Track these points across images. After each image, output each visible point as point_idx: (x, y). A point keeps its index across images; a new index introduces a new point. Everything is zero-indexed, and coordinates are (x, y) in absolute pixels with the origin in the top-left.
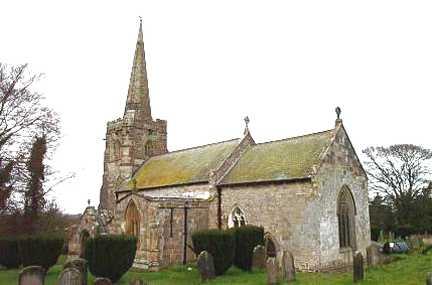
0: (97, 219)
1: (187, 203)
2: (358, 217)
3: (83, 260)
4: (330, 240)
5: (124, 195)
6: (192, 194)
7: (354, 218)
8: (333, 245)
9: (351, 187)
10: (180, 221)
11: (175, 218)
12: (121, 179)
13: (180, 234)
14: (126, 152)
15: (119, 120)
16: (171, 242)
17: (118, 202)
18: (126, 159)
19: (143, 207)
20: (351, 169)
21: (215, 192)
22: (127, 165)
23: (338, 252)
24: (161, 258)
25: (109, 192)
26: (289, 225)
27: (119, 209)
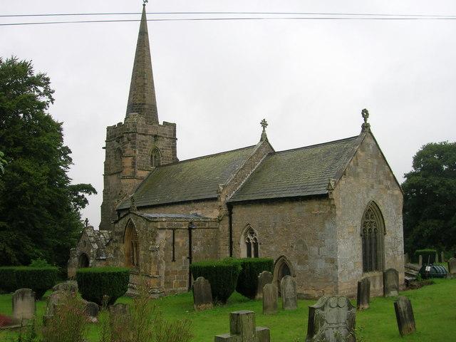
4: (351, 264)
7: (383, 239)
11: (177, 240)
13: (184, 258)
20: (380, 182)
24: (162, 284)
26: (305, 248)
27: (116, 230)
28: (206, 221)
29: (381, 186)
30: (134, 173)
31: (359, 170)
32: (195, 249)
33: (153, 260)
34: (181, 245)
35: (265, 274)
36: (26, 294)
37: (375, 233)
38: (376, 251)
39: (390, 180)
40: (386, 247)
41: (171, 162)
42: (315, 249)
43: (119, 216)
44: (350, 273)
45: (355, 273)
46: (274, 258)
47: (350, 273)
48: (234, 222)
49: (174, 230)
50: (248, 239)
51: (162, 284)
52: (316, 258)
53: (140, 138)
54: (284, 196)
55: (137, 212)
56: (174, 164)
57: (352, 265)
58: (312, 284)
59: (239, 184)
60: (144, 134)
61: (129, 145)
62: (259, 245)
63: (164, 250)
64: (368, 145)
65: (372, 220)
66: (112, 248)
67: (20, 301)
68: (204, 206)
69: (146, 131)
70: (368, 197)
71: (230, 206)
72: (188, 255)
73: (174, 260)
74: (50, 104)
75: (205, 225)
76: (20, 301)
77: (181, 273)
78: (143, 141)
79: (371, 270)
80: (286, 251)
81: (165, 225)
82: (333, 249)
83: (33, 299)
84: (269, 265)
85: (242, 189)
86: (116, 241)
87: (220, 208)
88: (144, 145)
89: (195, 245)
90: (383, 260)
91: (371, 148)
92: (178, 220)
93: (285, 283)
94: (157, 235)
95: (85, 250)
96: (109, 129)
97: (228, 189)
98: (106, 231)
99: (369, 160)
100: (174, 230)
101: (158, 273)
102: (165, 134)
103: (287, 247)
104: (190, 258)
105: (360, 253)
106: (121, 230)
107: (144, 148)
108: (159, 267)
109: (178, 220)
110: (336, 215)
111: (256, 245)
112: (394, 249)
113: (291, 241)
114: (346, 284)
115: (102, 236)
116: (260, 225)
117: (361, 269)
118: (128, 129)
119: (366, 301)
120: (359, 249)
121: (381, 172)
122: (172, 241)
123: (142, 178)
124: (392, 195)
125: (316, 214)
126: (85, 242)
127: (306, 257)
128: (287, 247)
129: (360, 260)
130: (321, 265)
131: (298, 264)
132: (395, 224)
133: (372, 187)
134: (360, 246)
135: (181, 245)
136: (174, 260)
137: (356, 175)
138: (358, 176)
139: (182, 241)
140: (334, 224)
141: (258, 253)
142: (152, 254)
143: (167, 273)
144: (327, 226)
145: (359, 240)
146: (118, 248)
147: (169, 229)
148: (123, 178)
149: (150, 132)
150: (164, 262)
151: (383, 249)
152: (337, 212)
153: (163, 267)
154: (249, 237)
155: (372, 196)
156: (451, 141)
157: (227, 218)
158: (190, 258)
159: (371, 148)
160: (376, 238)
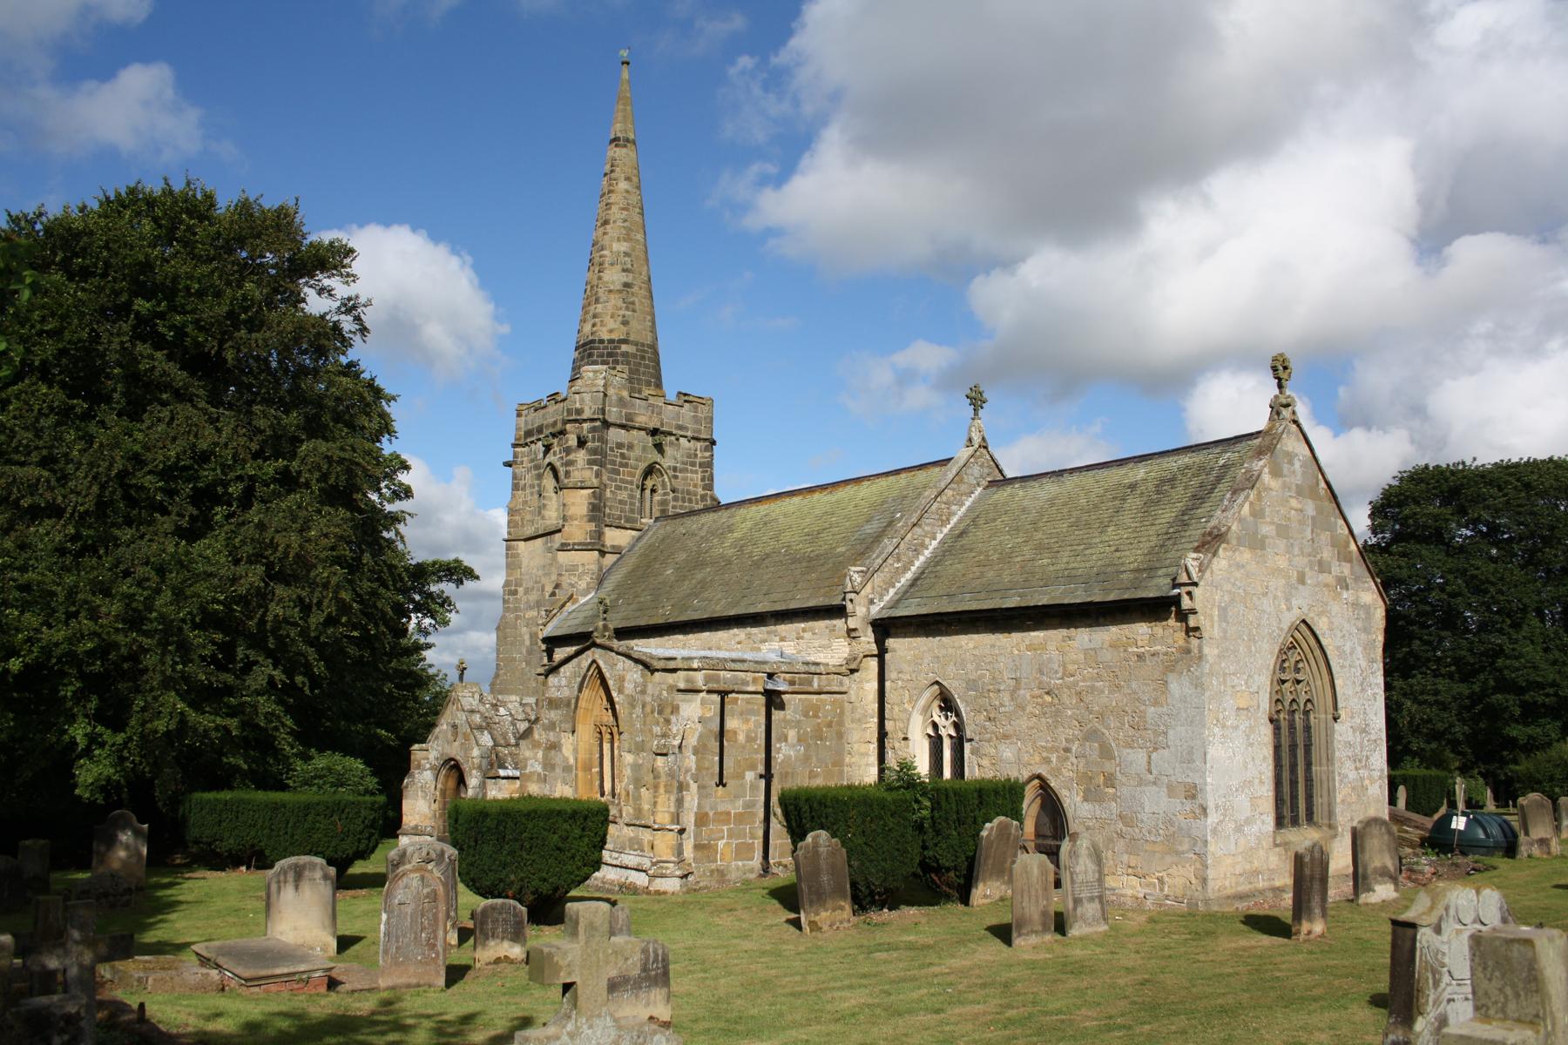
0: (488, 725)
1: (770, 676)
2: (1343, 731)
3: (344, 360)
4: (1242, 802)
5: (571, 650)
6: (789, 648)
7: (1329, 734)
8: (1248, 821)
9: (1321, 626)
10: (750, 739)
11: (731, 724)
12: (556, 599)
13: (750, 776)
14: (579, 502)
15: (553, 397)
16: (721, 800)
17: (553, 670)
18: (578, 530)
19: (629, 688)
20: (1323, 567)
21: (868, 640)
22: (585, 547)
23: (1267, 842)
24: (688, 852)
25: (1417, 893)
26: (1106, 752)
27: (553, 693)
28: (813, 670)
29: (1327, 578)
30: (599, 535)
31: (1266, 529)
32: (782, 752)
33: (663, 780)
34: (741, 738)
35: (1003, 828)
36: (307, 873)
37: (1306, 713)
38: (1309, 764)
39: (1350, 561)
40: (1337, 754)
41: (697, 507)
42: (1138, 758)
43: (550, 658)
44: (1239, 829)
45: (1255, 829)
46: (1020, 773)
47: (1239, 829)
48: (891, 674)
49: (723, 694)
50: (935, 726)
51: (688, 852)
52: (1141, 782)
53: (615, 435)
54: (1043, 600)
55: (615, 644)
56: (706, 510)
57: (1247, 804)
58: (1125, 858)
59: (906, 569)
60: (622, 426)
61: (581, 456)
62: (967, 746)
63: (696, 751)
64: (1290, 457)
65: (1299, 677)
66: (536, 745)
67: (288, 893)
68: (804, 630)
69: (629, 417)
70: (1289, 609)
71: (885, 628)
72: (761, 769)
73: (721, 783)
74: (357, 338)
75: (810, 683)
76: (288, 893)
77: (740, 818)
78: (620, 446)
79: (1295, 822)
80: (1047, 761)
81: (699, 679)
82: (1193, 756)
83: (326, 889)
84: (1004, 797)
85: (914, 582)
86: (552, 726)
87: (851, 633)
88: (623, 456)
89: (779, 740)
90: (1331, 792)
91: (1297, 465)
92: (733, 666)
93: (1074, 854)
94: (675, 710)
95: (454, 750)
96: (1336, 435)
97: (878, 579)
98: (513, 698)
99: (1294, 503)
100: (723, 694)
101: (676, 818)
102: (680, 427)
103: (1053, 749)
104: (768, 776)
105: (1267, 770)
106: (566, 693)
107: (622, 465)
108: (680, 802)
109: (733, 666)
110: (1201, 657)
111: (959, 743)
112: (1360, 762)
113: (1063, 734)
114: (1229, 861)
115: (502, 711)
116: (971, 684)
117: (1270, 820)
118: (579, 412)
119: (1317, 911)
120: (1265, 758)
121: (1325, 537)
122: (716, 728)
123: (617, 550)
124: (1356, 605)
125: (1140, 657)
126: (455, 726)
127: (1110, 780)
128: (1053, 749)
129: (1267, 791)
130: (1155, 803)
131: (1085, 799)
132: (1363, 690)
133: (1302, 580)
134: (1268, 752)
135: (741, 738)
136: (721, 783)
137: (1257, 544)
138: (1263, 548)
139: (745, 724)
140: (1198, 685)
141: (1312, 813)
142: (660, 761)
143: (701, 820)
144: (1175, 687)
145: (1266, 731)
146: (554, 746)
147: (709, 692)
148: (564, 548)
149: (641, 420)
150: (694, 787)
151: (1330, 760)
152: (1206, 650)
153: (692, 799)
154: (936, 719)
155: (1302, 604)
156: (1559, 453)
157: (873, 664)
158: (768, 776)
159: (1297, 465)
160: (1307, 728)
